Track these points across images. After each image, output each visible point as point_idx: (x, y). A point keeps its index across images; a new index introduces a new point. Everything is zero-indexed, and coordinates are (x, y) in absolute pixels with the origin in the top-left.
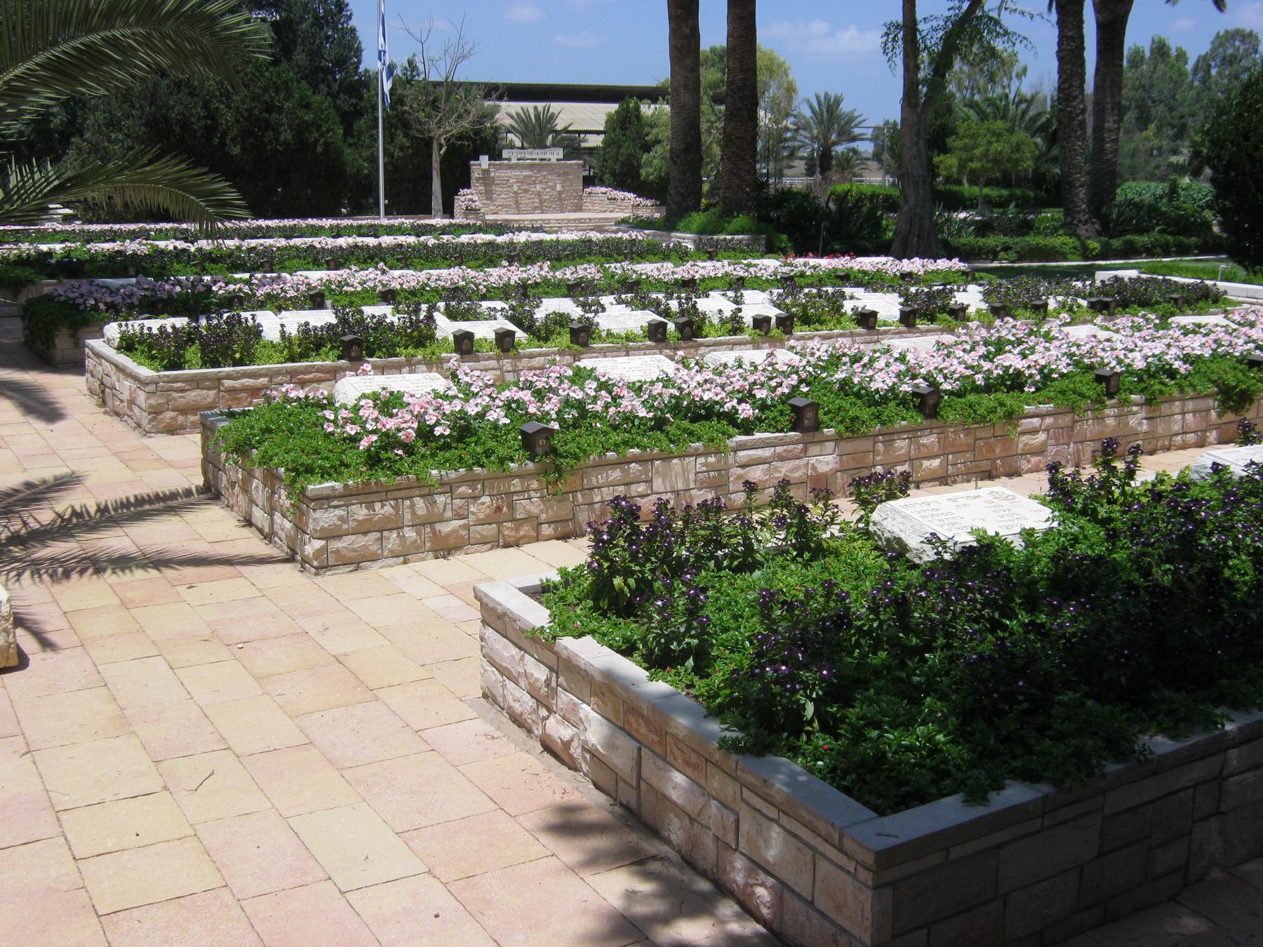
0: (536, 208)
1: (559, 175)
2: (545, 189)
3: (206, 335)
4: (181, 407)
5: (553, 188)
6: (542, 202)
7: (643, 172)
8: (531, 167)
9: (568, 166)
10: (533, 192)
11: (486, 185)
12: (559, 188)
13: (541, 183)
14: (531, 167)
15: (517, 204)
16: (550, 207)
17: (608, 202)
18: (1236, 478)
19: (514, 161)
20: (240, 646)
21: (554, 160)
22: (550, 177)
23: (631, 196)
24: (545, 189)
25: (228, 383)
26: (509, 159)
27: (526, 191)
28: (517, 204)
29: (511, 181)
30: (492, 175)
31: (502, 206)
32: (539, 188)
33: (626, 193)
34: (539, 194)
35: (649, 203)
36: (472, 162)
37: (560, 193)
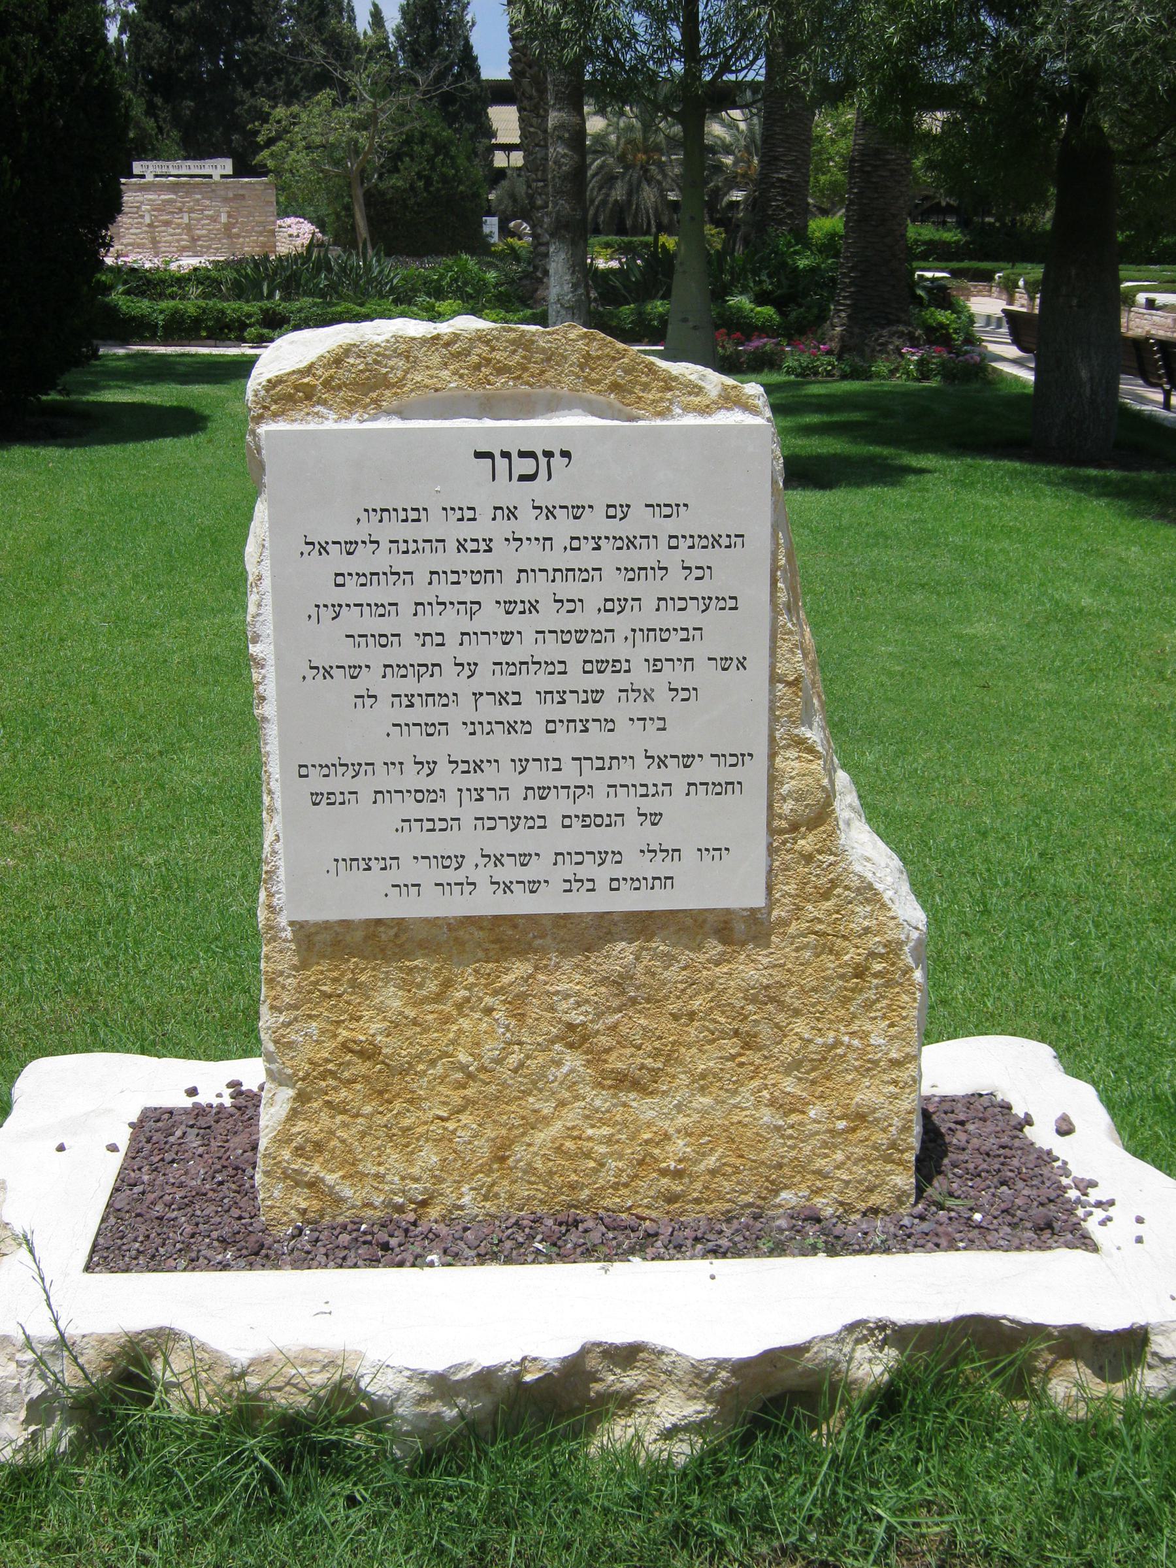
1: (226, 200)
5: (214, 219)
6: (194, 240)
10: (179, 226)
14: (173, 188)
15: (155, 242)
16: (209, 247)
19: (149, 178)
22: (208, 202)
26: (143, 176)
27: (167, 223)
28: (155, 242)
29: (144, 208)
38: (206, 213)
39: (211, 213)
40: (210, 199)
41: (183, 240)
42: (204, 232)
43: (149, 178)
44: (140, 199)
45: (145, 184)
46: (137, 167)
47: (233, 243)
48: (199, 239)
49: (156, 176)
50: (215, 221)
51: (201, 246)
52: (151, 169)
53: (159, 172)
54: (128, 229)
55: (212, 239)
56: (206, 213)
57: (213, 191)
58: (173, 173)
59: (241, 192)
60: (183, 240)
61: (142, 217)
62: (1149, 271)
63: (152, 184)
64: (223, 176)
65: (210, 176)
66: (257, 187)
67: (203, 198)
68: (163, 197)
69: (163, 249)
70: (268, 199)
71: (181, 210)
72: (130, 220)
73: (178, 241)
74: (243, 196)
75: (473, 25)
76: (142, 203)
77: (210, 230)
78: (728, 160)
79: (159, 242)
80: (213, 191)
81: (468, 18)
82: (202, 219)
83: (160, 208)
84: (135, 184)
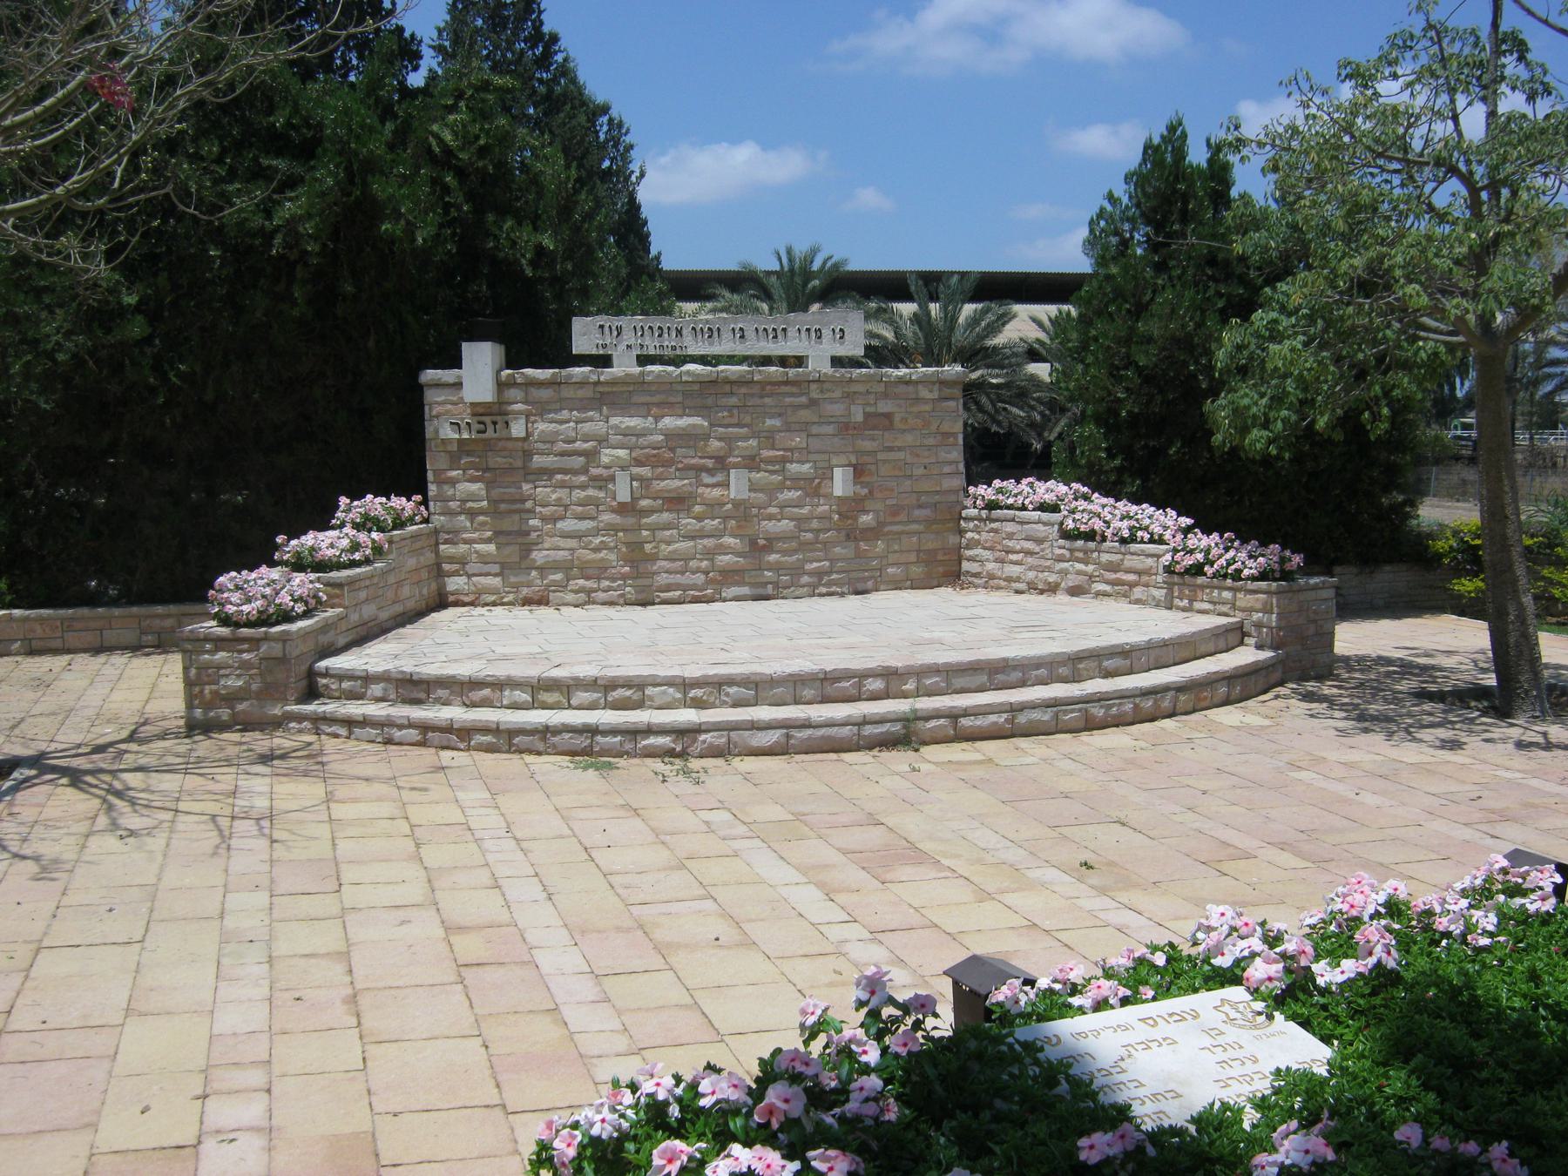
0: (729, 576)
2: (771, 491)
3: (856, 519)
4: (716, 454)
5: (814, 487)
6: (757, 548)
7: (1219, 410)
8: (702, 395)
9: (890, 390)
10: (713, 507)
11: (491, 475)
12: (841, 482)
13: (752, 463)
14: (702, 395)
15: (638, 558)
16: (797, 571)
17: (1060, 547)
18: (1322, 1071)
19: (624, 367)
20: (44, 1026)
21: (819, 362)
23: (1166, 521)
24: (771, 491)
25: (692, 453)
26: (604, 361)
27: (678, 502)
28: (638, 558)
29: (607, 456)
30: (517, 429)
31: (566, 567)
32: (738, 485)
33: (1145, 512)
34: (743, 513)
35: (1247, 559)
36: (429, 375)
37: (850, 508)
38: (794, 468)
39: (806, 468)
40: (804, 428)
41: (724, 550)
42: (786, 525)
43: (624, 367)
44: (598, 427)
45: (614, 382)
46: (585, 334)
47: (859, 555)
48: (769, 548)
49: (643, 360)
50: (816, 493)
51: (777, 568)
52: (628, 338)
53: (651, 346)
54: (554, 519)
55: (804, 546)
56: (794, 468)
57: (813, 403)
58: (693, 350)
59: (884, 407)
60: (724, 550)
61: (604, 482)
62: (1457, 508)
63: (639, 383)
64: (837, 362)
65: (800, 361)
66: (924, 393)
67: (788, 428)
68: (668, 422)
69: (663, 579)
70: (946, 427)
71: (721, 464)
72: (561, 493)
73: (710, 554)
74: (888, 416)
75: (642, 175)
76: (603, 441)
77: (799, 520)
78: (1041, 370)
79: (654, 558)
80: (813, 403)
81: (635, 167)
82: (781, 487)
83: (659, 458)
84: (583, 384)
